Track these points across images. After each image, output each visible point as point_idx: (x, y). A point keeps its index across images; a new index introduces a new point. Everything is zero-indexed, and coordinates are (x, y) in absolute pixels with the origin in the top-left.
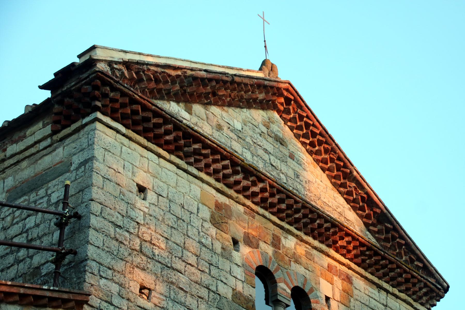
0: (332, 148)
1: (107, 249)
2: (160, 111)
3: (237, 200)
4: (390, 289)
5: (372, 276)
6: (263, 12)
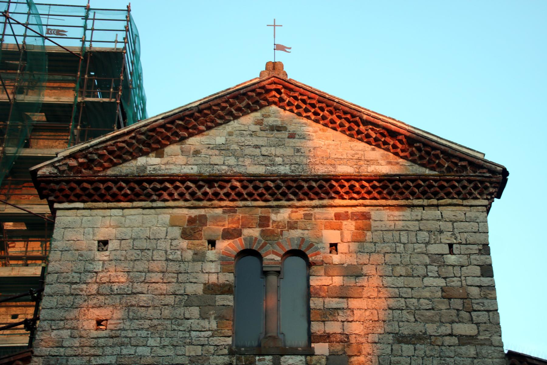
0: (334, 108)
1: (60, 306)
2: (104, 178)
3: (213, 206)
4: (425, 202)
5: (397, 201)
6: (275, 20)
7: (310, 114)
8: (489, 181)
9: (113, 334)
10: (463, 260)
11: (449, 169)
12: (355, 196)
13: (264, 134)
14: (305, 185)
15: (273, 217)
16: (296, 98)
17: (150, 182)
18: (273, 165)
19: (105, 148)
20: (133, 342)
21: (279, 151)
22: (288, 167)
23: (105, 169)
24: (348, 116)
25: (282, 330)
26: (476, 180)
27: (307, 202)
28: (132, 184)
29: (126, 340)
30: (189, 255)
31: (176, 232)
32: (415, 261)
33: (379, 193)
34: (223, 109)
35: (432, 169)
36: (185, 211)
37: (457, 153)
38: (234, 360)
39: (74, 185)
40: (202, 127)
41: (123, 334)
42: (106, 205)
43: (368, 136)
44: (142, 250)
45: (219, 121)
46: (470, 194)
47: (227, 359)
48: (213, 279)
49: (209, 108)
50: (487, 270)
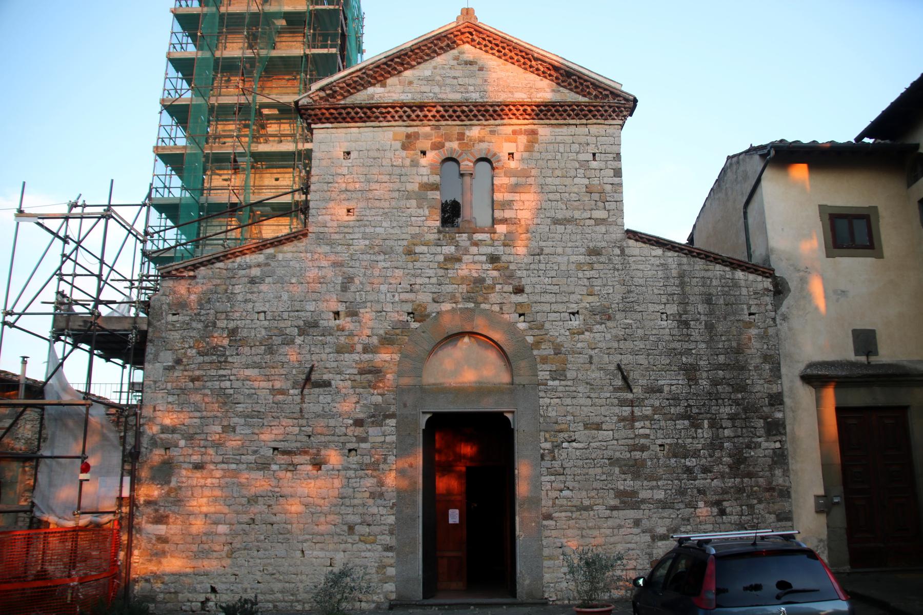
4: (578, 122)
7: (494, 51)
8: (628, 105)
9: (358, 218)
10: (602, 165)
11: (596, 97)
12: (527, 117)
13: (460, 67)
14: (491, 109)
15: (468, 133)
16: (484, 39)
17: (377, 108)
18: (467, 92)
19: (344, 82)
20: (373, 224)
21: (472, 81)
22: (478, 94)
23: (345, 97)
24: (523, 54)
25: (474, 215)
26: (612, 105)
27: (492, 122)
28: (365, 110)
29: (368, 223)
30: (408, 162)
31: (398, 145)
32: (568, 166)
33: (545, 115)
34: (429, 48)
35: (584, 96)
36: (404, 129)
37: (602, 85)
38: (441, 236)
39: (324, 111)
40: (414, 63)
41: (366, 218)
42: (347, 125)
43: (538, 69)
44: (374, 159)
45: (426, 58)
46: (610, 116)
47: (436, 236)
48: (425, 179)
49: (419, 48)
50: (618, 173)
